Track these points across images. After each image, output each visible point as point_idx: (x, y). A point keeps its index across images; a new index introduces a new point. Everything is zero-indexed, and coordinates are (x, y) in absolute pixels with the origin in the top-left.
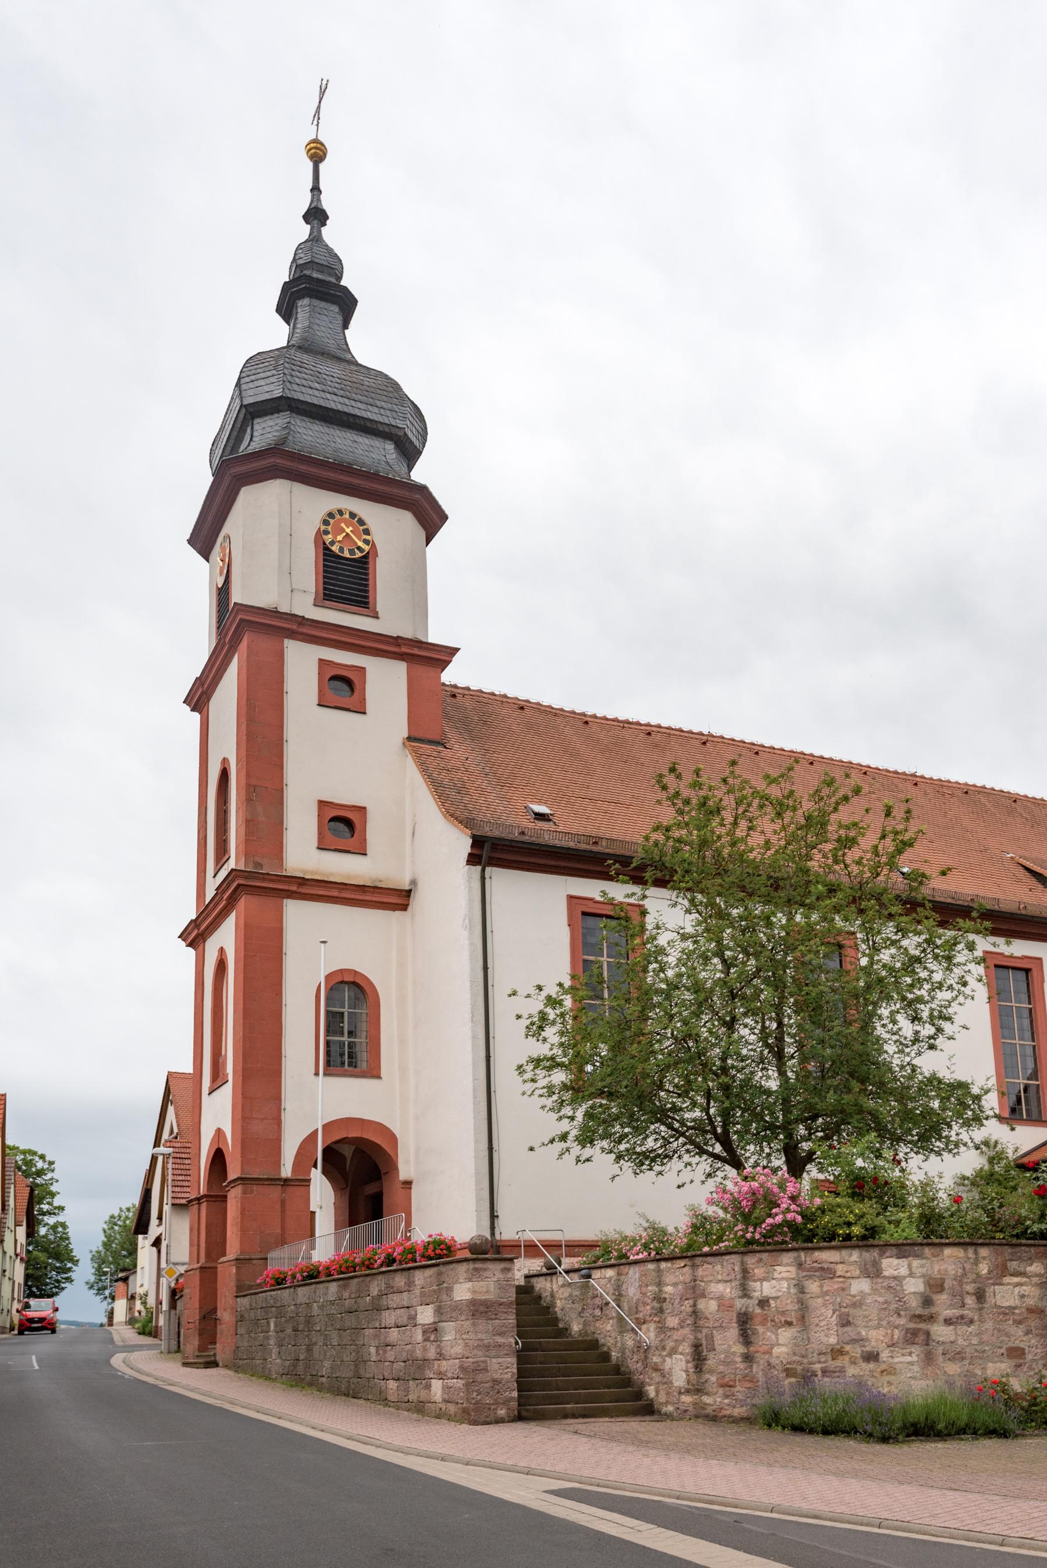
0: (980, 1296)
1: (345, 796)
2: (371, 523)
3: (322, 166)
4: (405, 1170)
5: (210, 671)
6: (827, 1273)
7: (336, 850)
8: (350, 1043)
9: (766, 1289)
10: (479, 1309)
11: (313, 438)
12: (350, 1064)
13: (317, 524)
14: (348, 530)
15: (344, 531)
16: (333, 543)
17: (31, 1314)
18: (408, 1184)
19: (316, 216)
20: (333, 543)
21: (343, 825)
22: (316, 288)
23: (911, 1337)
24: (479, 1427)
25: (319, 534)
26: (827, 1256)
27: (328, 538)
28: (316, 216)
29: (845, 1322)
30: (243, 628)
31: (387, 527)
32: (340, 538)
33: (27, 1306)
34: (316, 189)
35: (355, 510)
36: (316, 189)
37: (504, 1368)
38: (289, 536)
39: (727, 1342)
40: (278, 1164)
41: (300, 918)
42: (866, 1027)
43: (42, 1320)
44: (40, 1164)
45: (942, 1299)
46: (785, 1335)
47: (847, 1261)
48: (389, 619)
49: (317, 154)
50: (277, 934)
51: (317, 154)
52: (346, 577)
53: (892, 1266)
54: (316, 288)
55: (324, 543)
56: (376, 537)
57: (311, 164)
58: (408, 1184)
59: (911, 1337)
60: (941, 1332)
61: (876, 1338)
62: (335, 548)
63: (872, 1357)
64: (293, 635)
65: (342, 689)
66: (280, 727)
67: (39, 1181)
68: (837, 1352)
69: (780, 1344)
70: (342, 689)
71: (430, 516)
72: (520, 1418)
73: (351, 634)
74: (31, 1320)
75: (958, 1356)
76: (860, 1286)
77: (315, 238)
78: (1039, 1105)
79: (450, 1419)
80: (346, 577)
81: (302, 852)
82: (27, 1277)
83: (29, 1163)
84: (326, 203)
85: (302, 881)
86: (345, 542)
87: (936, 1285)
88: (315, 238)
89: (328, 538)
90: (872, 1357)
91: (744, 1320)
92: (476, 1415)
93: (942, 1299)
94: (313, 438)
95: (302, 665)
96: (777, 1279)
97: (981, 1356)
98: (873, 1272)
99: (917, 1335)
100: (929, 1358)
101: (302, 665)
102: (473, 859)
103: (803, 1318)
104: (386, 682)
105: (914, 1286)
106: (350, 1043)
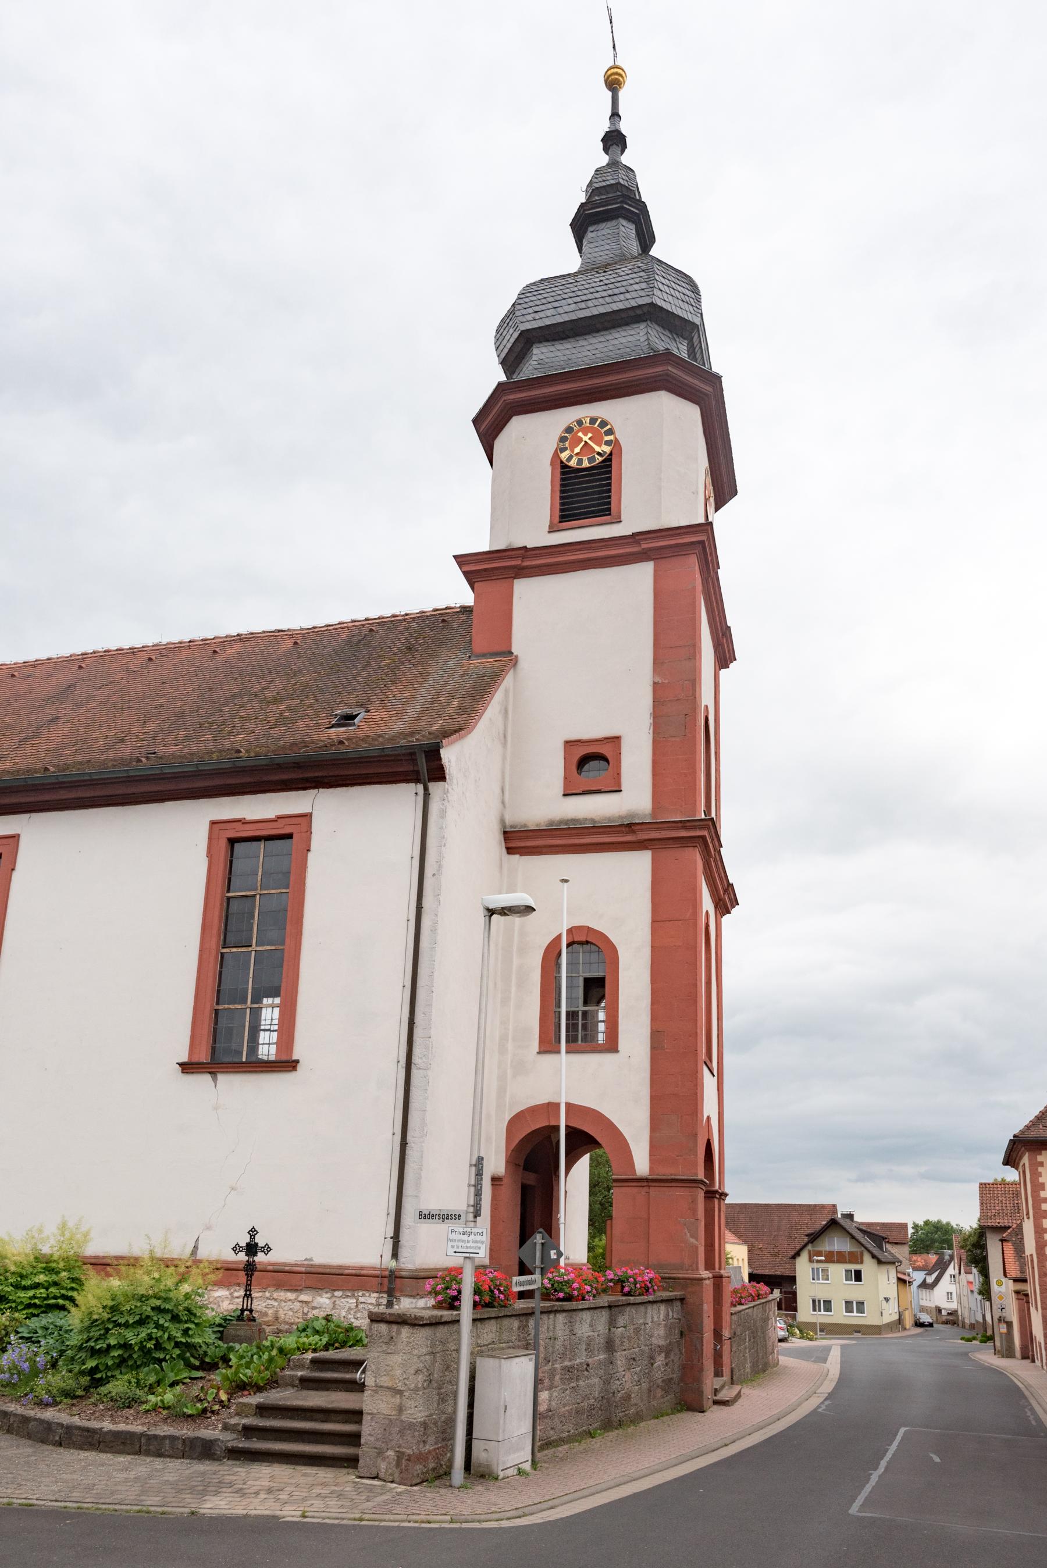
3: (622, 94)
5: (715, 594)
7: (584, 793)
8: (585, 1013)
12: (585, 1039)
13: (553, 445)
14: (586, 438)
15: (581, 440)
16: (570, 458)
19: (614, 141)
20: (570, 458)
24: (767, 1272)
25: (556, 455)
27: (564, 456)
28: (614, 141)
32: (577, 450)
34: (615, 115)
35: (594, 414)
36: (615, 115)
49: (614, 83)
51: (614, 83)
54: (612, 207)
55: (562, 462)
57: (609, 94)
62: (573, 463)
73: (672, 536)
77: (614, 164)
78: (471, 1405)
79: (658, 1415)
84: (624, 127)
88: (614, 164)
89: (564, 456)
106: (585, 1013)
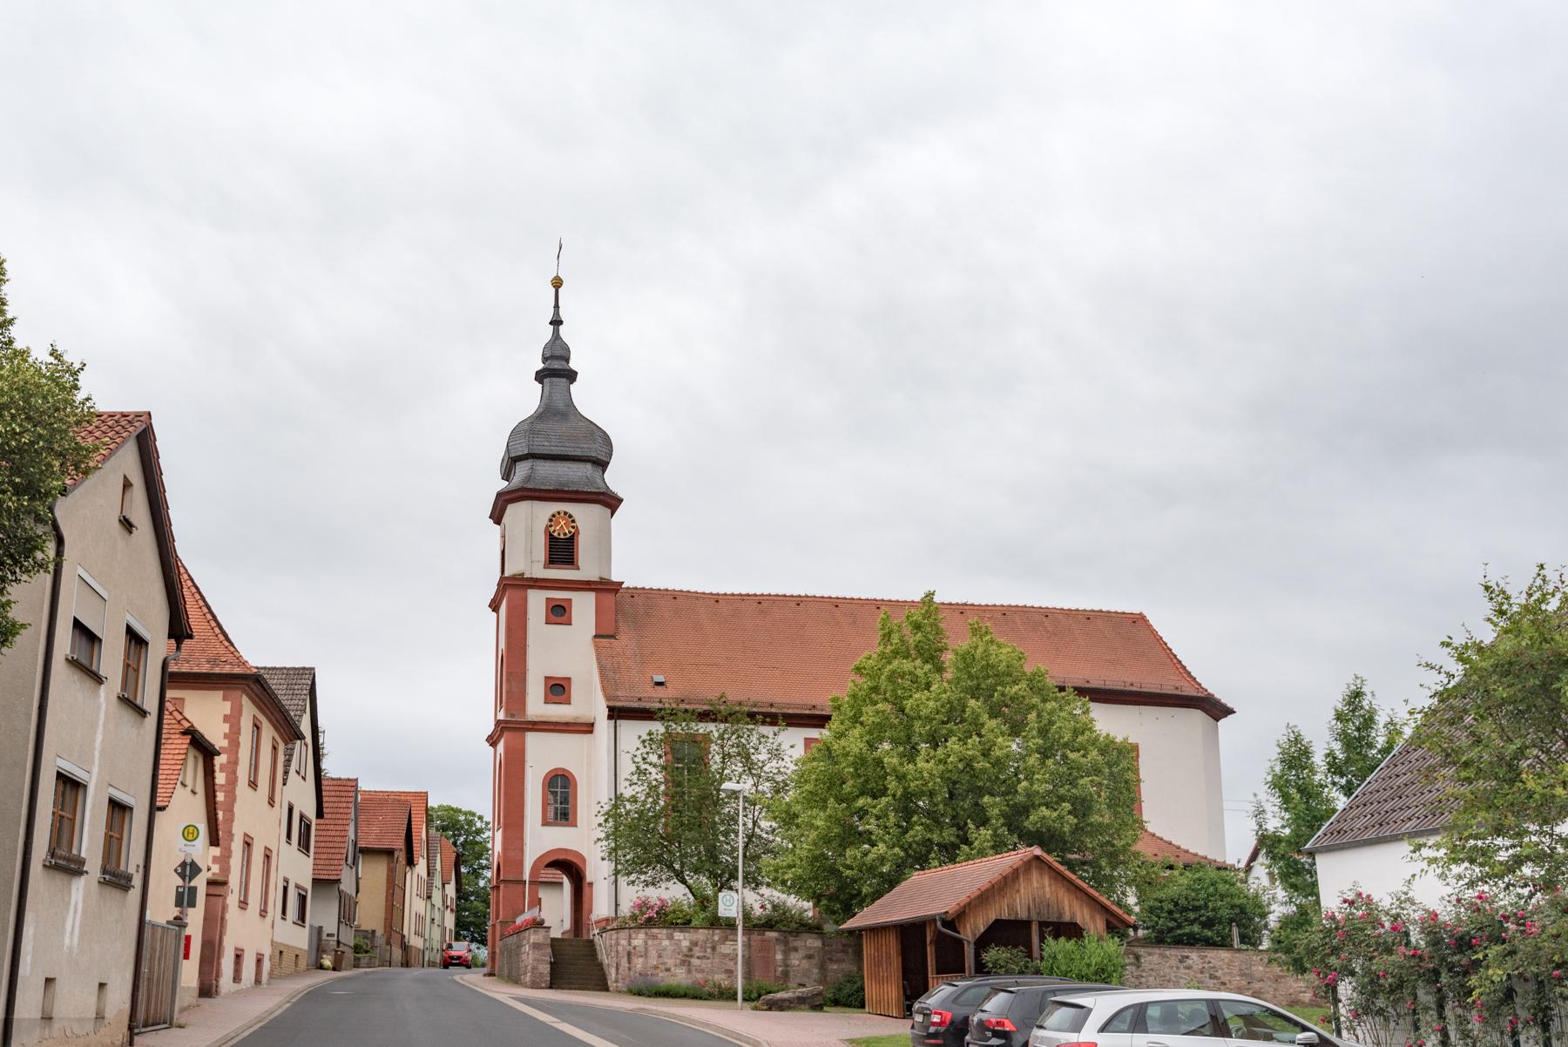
0: (714, 948)
1: (559, 673)
2: (576, 517)
4: (589, 878)
6: (655, 937)
9: (635, 943)
10: (536, 946)
11: (550, 473)
13: (546, 522)
17: (453, 953)
18: (591, 884)
19: (556, 322)
21: (558, 689)
22: (556, 370)
23: (683, 963)
26: (655, 931)
29: (660, 956)
30: (512, 587)
31: (585, 515)
33: (450, 946)
34: (557, 306)
36: (557, 306)
37: (545, 969)
38: (530, 532)
39: (624, 962)
40: (521, 873)
41: (533, 740)
42: (1560, 608)
43: (459, 958)
44: (479, 824)
45: (696, 949)
46: (641, 960)
47: (661, 933)
48: (586, 570)
49: (557, 283)
50: (522, 751)
51: (557, 283)
52: (562, 550)
53: (678, 935)
54: (556, 370)
56: (579, 524)
58: (591, 884)
59: (683, 963)
60: (695, 962)
61: (670, 962)
63: (668, 970)
64: (531, 587)
65: (559, 613)
66: (525, 639)
67: (478, 839)
68: (656, 967)
69: (639, 963)
70: (559, 613)
71: (611, 502)
72: (551, 988)
74: (452, 958)
75: (702, 971)
76: (666, 943)
77: (556, 336)
80: (562, 550)
81: (537, 706)
82: (457, 925)
83: (470, 823)
85: (535, 723)
86: (562, 529)
87: (695, 944)
88: (556, 336)
90: (668, 970)
91: (629, 954)
92: (535, 985)
93: (696, 949)
94: (550, 473)
95: (537, 601)
96: (639, 939)
97: (712, 972)
98: (671, 937)
99: (685, 962)
100: (689, 971)
101: (537, 601)
102: (610, 717)
103: (646, 955)
104: (584, 606)
105: (686, 944)
